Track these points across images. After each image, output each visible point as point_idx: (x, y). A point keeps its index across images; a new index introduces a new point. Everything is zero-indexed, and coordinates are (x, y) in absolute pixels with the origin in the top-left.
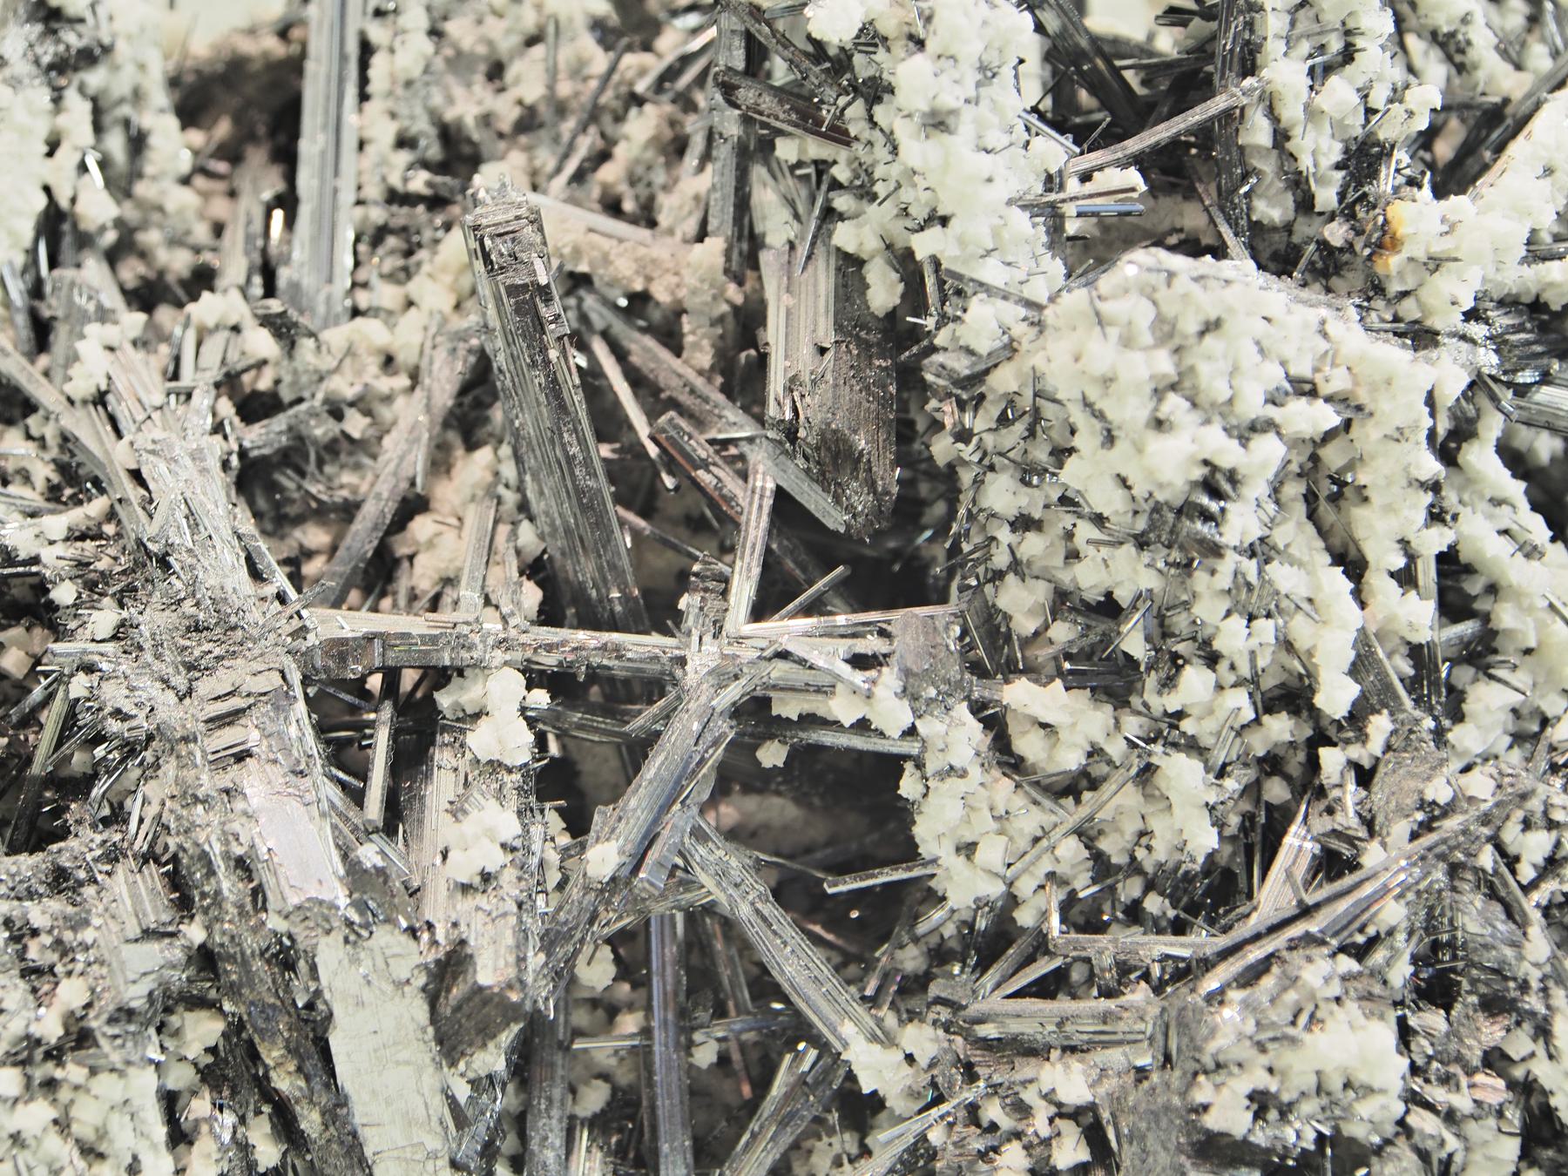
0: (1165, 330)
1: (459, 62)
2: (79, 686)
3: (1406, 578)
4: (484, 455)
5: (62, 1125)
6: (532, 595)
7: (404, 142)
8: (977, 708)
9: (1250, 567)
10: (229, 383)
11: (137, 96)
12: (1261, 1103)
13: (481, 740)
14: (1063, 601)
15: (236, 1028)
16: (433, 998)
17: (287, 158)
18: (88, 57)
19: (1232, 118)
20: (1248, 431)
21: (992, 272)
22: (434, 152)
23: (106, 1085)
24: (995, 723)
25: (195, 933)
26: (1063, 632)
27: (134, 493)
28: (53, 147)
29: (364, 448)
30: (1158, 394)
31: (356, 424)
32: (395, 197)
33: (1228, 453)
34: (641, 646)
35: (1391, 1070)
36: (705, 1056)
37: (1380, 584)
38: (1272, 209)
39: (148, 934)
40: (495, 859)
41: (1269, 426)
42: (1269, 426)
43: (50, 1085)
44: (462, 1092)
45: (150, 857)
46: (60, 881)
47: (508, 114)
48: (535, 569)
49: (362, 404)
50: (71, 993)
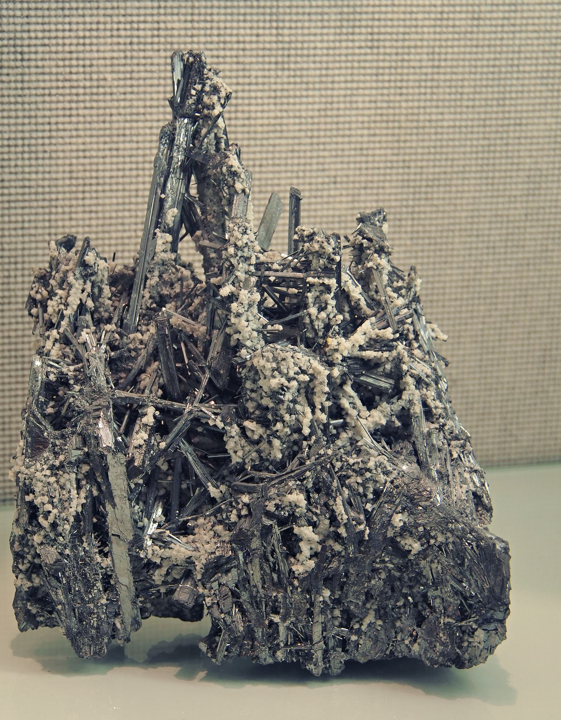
0: (275, 359)
1: (165, 283)
2: (72, 400)
3: (322, 410)
4: (157, 363)
5: (57, 482)
6: (160, 392)
7: (151, 297)
8: (239, 425)
9: (292, 405)
10: (109, 344)
11: (102, 281)
12: (277, 506)
13: (145, 420)
14: (259, 406)
15: (91, 469)
16: (127, 467)
17: (129, 295)
18: (92, 275)
19: (302, 318)
20: (289, 380)
21: (248, 343)
22: (157, 299)
23: (66, 475)
24: (243, 430)
25: (86, 450)
26: (257, 412)
27: (87, 364)
28: (83, 291)
29: (135, 358)
30: (273, 370)
31: (133, 354)
32: (148, 308)
33: (286, 383)
34: (177, 405)
35: (303, 503)
36: (184, 486)
37: (318, 412)
38: (310, 335)
39: (77, 449)
40: (142, 442)
41: (294, 379)
42: (294, 379)
43: (56, 475)
44: (133, 486)
45: (80, 434)
46: (63, 437)
47: (173, 294)
48: (162, 387)
49: (136, 350)
50: (62, 457)
